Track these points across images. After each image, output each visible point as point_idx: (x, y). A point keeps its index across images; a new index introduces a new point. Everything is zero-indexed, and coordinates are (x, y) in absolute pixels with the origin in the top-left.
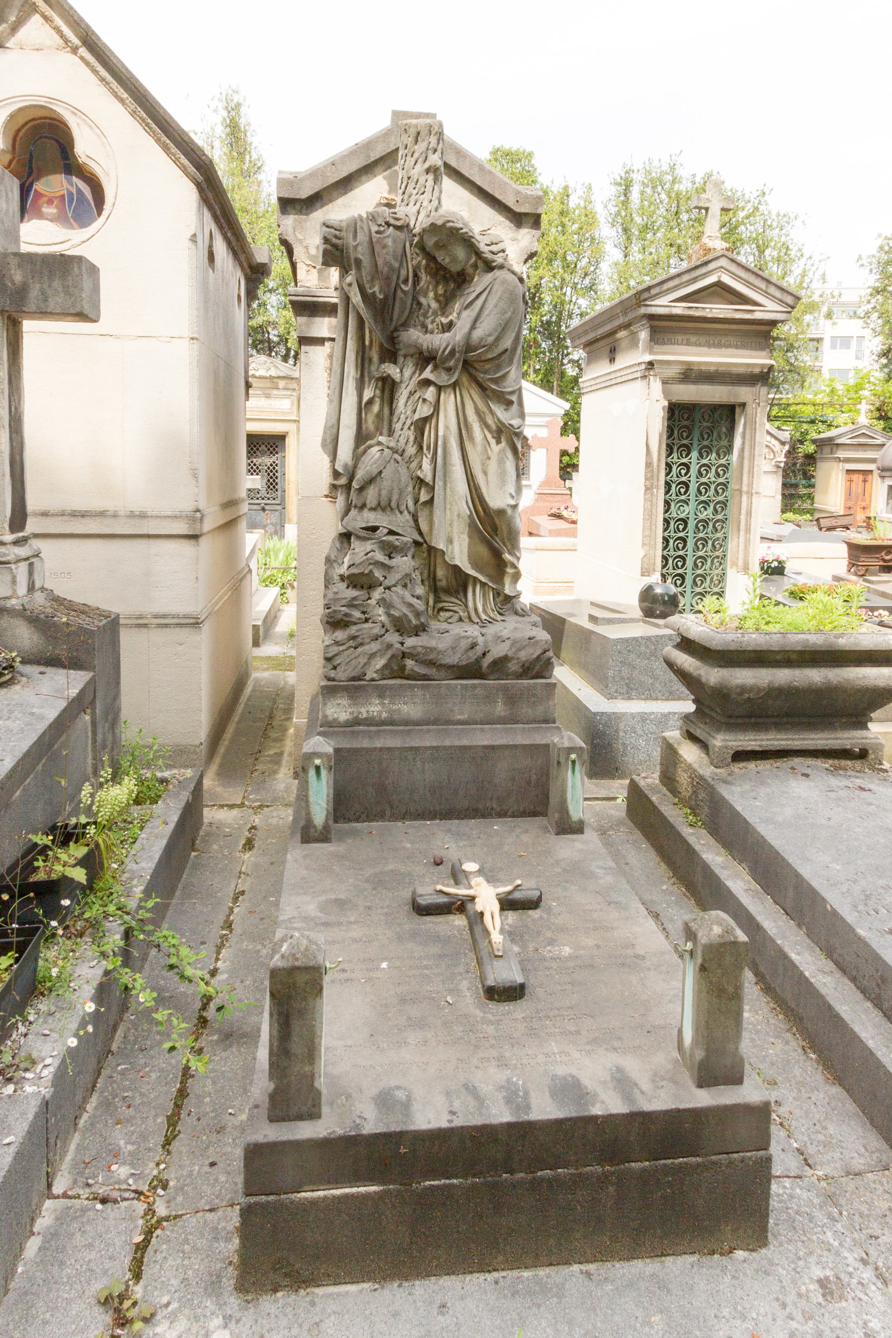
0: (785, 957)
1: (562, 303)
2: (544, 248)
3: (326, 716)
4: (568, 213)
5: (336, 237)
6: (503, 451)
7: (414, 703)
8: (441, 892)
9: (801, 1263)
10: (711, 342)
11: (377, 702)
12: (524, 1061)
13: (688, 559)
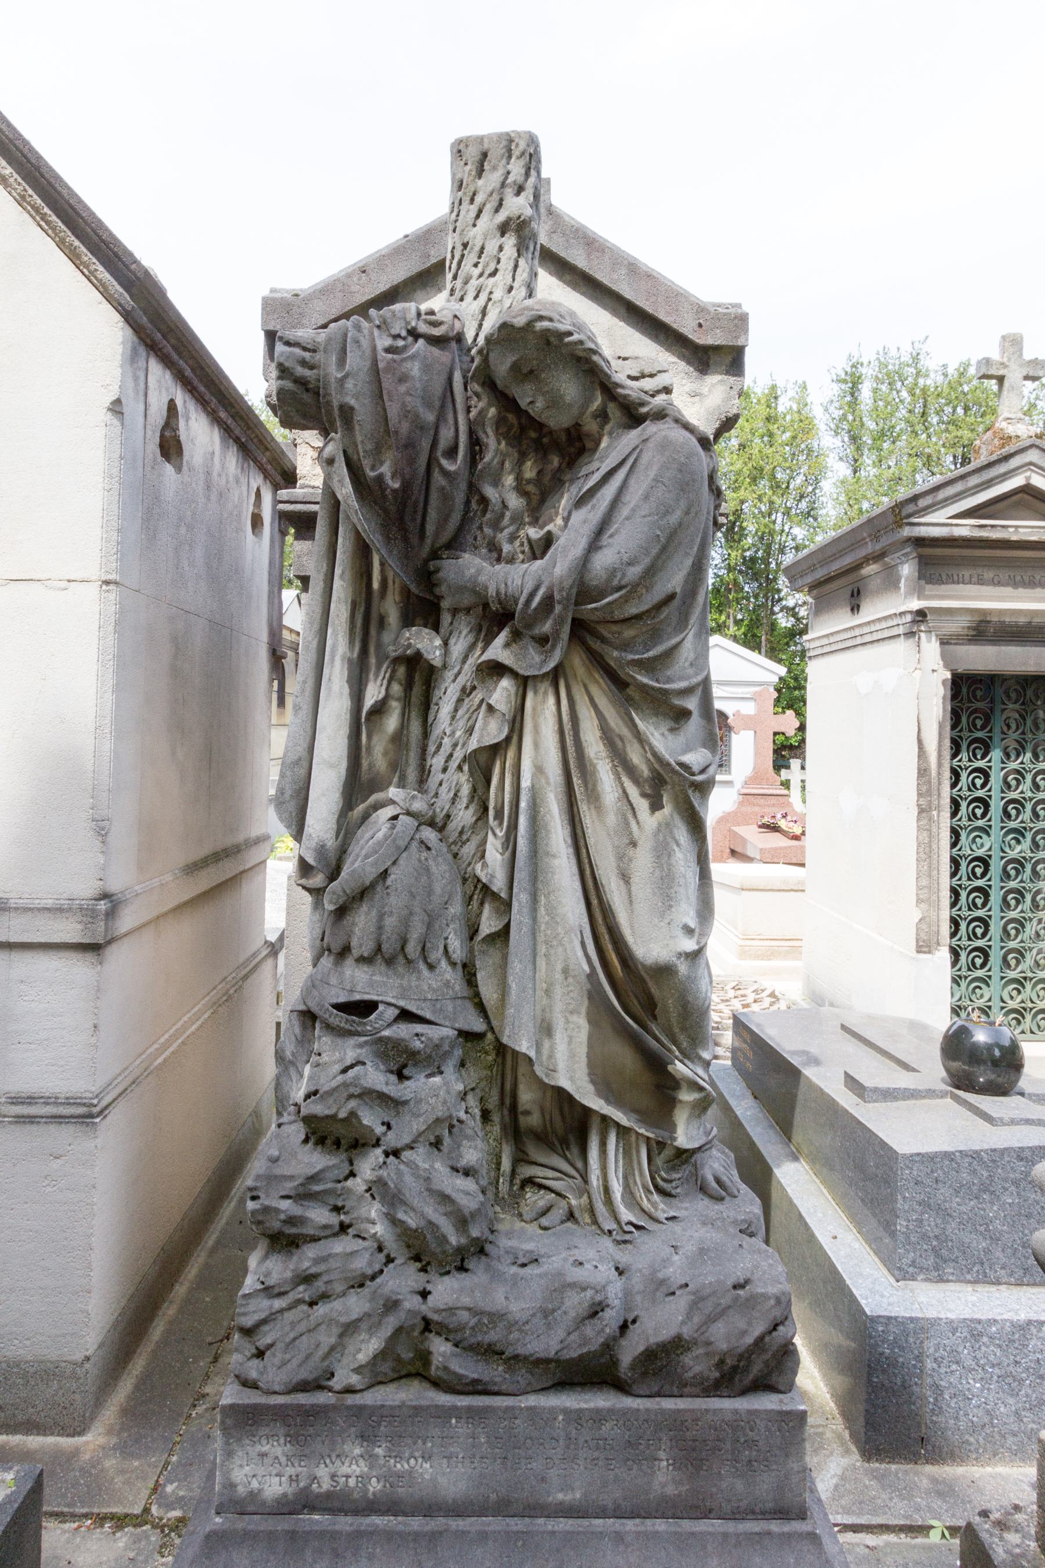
1: (771, 533)
2: (745, 463)
3: (232, 1486)
4: (776, 420)
5: (303, 363)
6: (666, 827)
7: (449, 1458)
10: (1018, 578)
11: (357, 1451)
13: (992, 923)
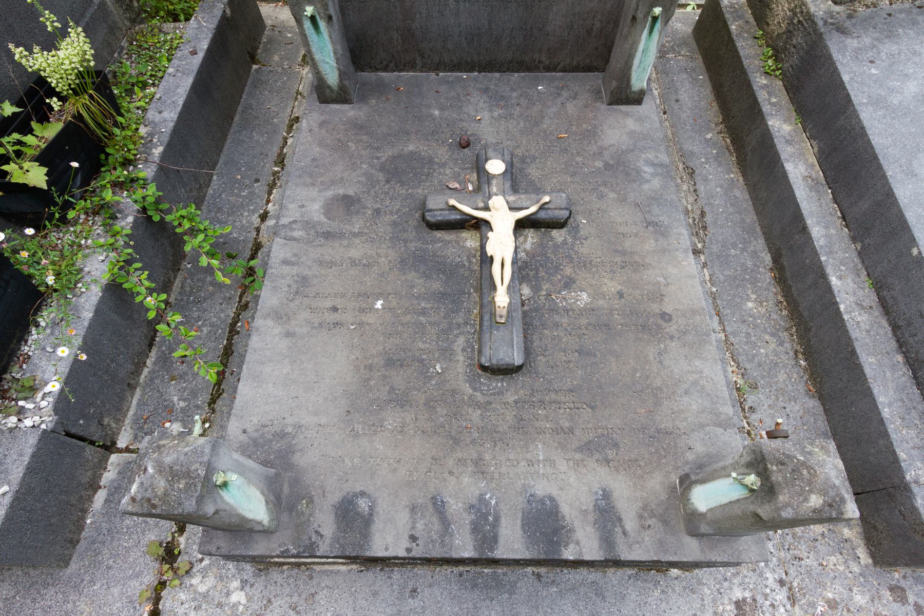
0: (824, 276)
8: (454, 208)
9: (726, 584)
12: (504, 469)
